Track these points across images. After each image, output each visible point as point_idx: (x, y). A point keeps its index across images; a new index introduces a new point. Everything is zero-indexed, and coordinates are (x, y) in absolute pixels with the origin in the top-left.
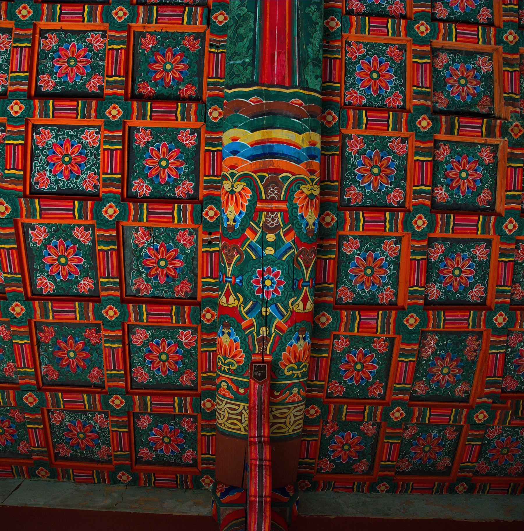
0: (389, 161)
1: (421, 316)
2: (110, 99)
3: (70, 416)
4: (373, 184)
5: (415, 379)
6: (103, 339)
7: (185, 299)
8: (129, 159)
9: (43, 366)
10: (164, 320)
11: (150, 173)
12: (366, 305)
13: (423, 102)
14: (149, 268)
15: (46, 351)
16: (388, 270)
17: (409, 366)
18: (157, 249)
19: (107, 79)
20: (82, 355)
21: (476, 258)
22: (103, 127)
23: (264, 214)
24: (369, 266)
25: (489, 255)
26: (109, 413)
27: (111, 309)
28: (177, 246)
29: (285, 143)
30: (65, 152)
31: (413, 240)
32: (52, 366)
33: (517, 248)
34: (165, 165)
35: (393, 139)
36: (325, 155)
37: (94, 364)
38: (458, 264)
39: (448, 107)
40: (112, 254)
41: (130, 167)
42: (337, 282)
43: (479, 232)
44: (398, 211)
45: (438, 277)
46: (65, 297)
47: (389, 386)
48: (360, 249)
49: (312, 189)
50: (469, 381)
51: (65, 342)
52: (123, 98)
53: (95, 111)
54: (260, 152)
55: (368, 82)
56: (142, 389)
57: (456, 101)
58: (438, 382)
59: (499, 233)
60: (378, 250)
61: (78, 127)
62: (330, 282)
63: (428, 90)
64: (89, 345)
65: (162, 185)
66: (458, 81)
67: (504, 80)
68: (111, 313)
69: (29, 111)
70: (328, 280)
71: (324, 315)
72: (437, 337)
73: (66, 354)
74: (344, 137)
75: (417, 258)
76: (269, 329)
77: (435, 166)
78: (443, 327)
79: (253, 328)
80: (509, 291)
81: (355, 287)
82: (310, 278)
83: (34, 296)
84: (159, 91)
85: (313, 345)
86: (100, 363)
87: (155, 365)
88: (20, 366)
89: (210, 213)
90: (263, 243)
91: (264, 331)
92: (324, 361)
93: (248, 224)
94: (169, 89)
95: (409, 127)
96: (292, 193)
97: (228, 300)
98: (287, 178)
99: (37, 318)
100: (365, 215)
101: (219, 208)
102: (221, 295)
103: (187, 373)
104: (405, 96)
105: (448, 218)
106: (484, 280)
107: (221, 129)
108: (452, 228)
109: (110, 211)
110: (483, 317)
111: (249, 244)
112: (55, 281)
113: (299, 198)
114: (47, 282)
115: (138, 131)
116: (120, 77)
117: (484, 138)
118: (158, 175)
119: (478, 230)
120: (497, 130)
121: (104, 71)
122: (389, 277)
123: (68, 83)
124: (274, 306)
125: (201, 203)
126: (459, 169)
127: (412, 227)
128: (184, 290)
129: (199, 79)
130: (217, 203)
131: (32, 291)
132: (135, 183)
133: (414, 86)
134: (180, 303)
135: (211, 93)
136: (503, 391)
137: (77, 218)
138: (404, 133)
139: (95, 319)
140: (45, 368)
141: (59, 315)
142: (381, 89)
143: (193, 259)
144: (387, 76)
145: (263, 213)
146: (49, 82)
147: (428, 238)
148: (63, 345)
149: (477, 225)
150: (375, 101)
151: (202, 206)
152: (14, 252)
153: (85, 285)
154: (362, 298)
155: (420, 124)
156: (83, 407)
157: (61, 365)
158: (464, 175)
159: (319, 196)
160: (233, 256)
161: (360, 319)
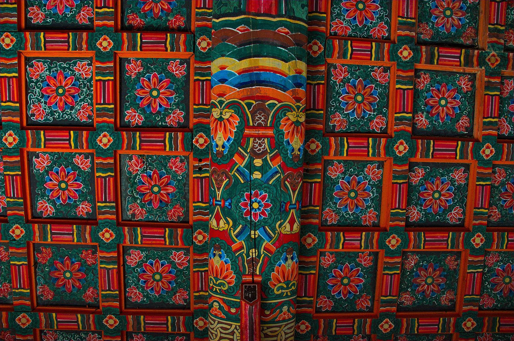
0: (372, 90)
1: (402, 237)
2: (101, 31)
3: (63, 336)
4: (357, 111)
5: (401, 290)
6: (99, 260)
7: (178, 223)
8: (121, 90)
9: (38, 287)
10: (158, 242)
11: (142, 103)
12: (350, 226)
13: (407, 32)
14: (144, 194)
15: (42, 271)
16: (371, 193)
17: (394, 278)
18: (150, 176)
19: (97, 10)
20: (78, 275)
21: (455, 182)
22: (94, 59)
23: (251, 140)
24: (353, 189)
25: (467, 179)
26: (103, 332)
27: (107, 231)
28: (169, 172)
29: (271, 71)
30: (58, 84)
31: (395, 165)
32: (48, 286)
33: (494, 173)
34: (155, 95)
35: (375, 68)
36: (311, 84)
37: (89, 284)
38: (437, 188)
39: (432, 38)
40: (109, 180)
41: (123, 97)
42: (323, 205)
43: (458, 157)
44: (381, 137)
45: (418, 200)
46: (63, 220)
47: (376, 298)
48: (344, 173)
49: (298, 116)
50: (454, 289)
51: (62, 263)
52: (113, 29)
53: (86, 43)
54: (247, 80)
55: (354, 12)
56: (136, 309)
57: (441, 32)
58: (423, 292)
59: (477, 158)
60: (361, 174)
61: (70, 59)
62: (316, 204)
63: (413, 21)
64: (85, 266)
65: (154, 114)
66: (444, 13)
67: (490, 11)
68: (107, 235)
69: (21, 44)
70: (314, 203)
71: (310, 236)
72: (417, 257)
73: (61, 274)
74: (329, 66)
75: (399, 181)
76: (258, 251)
77: (416, 94)
78: (424, 248)
79: (243, 250)
80: (486, 213)
81: (339, 209)
82: (297, 201)
83: (35, 219)
84: (149, 22)
85: (300, 262)
86: (95, 283)
87: (149, 285)
88: (15, 287)
89: (200, 140)
90: (251, 167)
91: (253, 253)
92: (312, 278)
93: (236, 149)
94: (158, 20)
95: (391, 57)
96: (278, 120)
97: (218, 224)
98: (273, 105)
99: (36, 240)
100: (349, 141)
101: (208, 136)
102: (211, 218)
103: (180, 292)
104: (390, 27)
105: (429, 144)
106: (462, 203)
107: (209, 59)
108: (432, 153)
109: (105, 140)
110: (461, 238)
111: (237, 169)
112: (54, 204)
113: (285, 125)
114: (47, 206)
115: (129, 62)
116: (109, 8)
117: (463, 67)
118: (149, 105)
119: (456, 155)
120: (475, 59)
121: (93, 3)
122: (372, 200)
123: (58, 15)
124: (262, 229)
125: (191, 131)
126: (438, 97)
127: (394, 152)
128: (176, 214)
129: (187, 10)
130: (206, 130)
131: (32, 214)
132: (127, 112)
133: (399, 17)
134: (173, 226)
135: (199, 23)
136: (480, 309)
137: (73, 148)
138: (386, 63)
139: (91, 241)
140: (40, 288)
141: (57, 237)
142: (366, 19)
143: (185, 185)
144: (373, 7)
145: (251, 139)
146: (38, 14)
147: (410, 163)
148: (59, 265)
149: (456, 151)
150: (360, 31)
151: (192, 134)
152: (18, 178)
153: (84, 209)
154: (346, 220)
155: (402, 54)
156: (77, 327)
157: (57, 285)
158: (443, 102)
159: (304, 123)
160: (222, 181)
161: (345, 240)
